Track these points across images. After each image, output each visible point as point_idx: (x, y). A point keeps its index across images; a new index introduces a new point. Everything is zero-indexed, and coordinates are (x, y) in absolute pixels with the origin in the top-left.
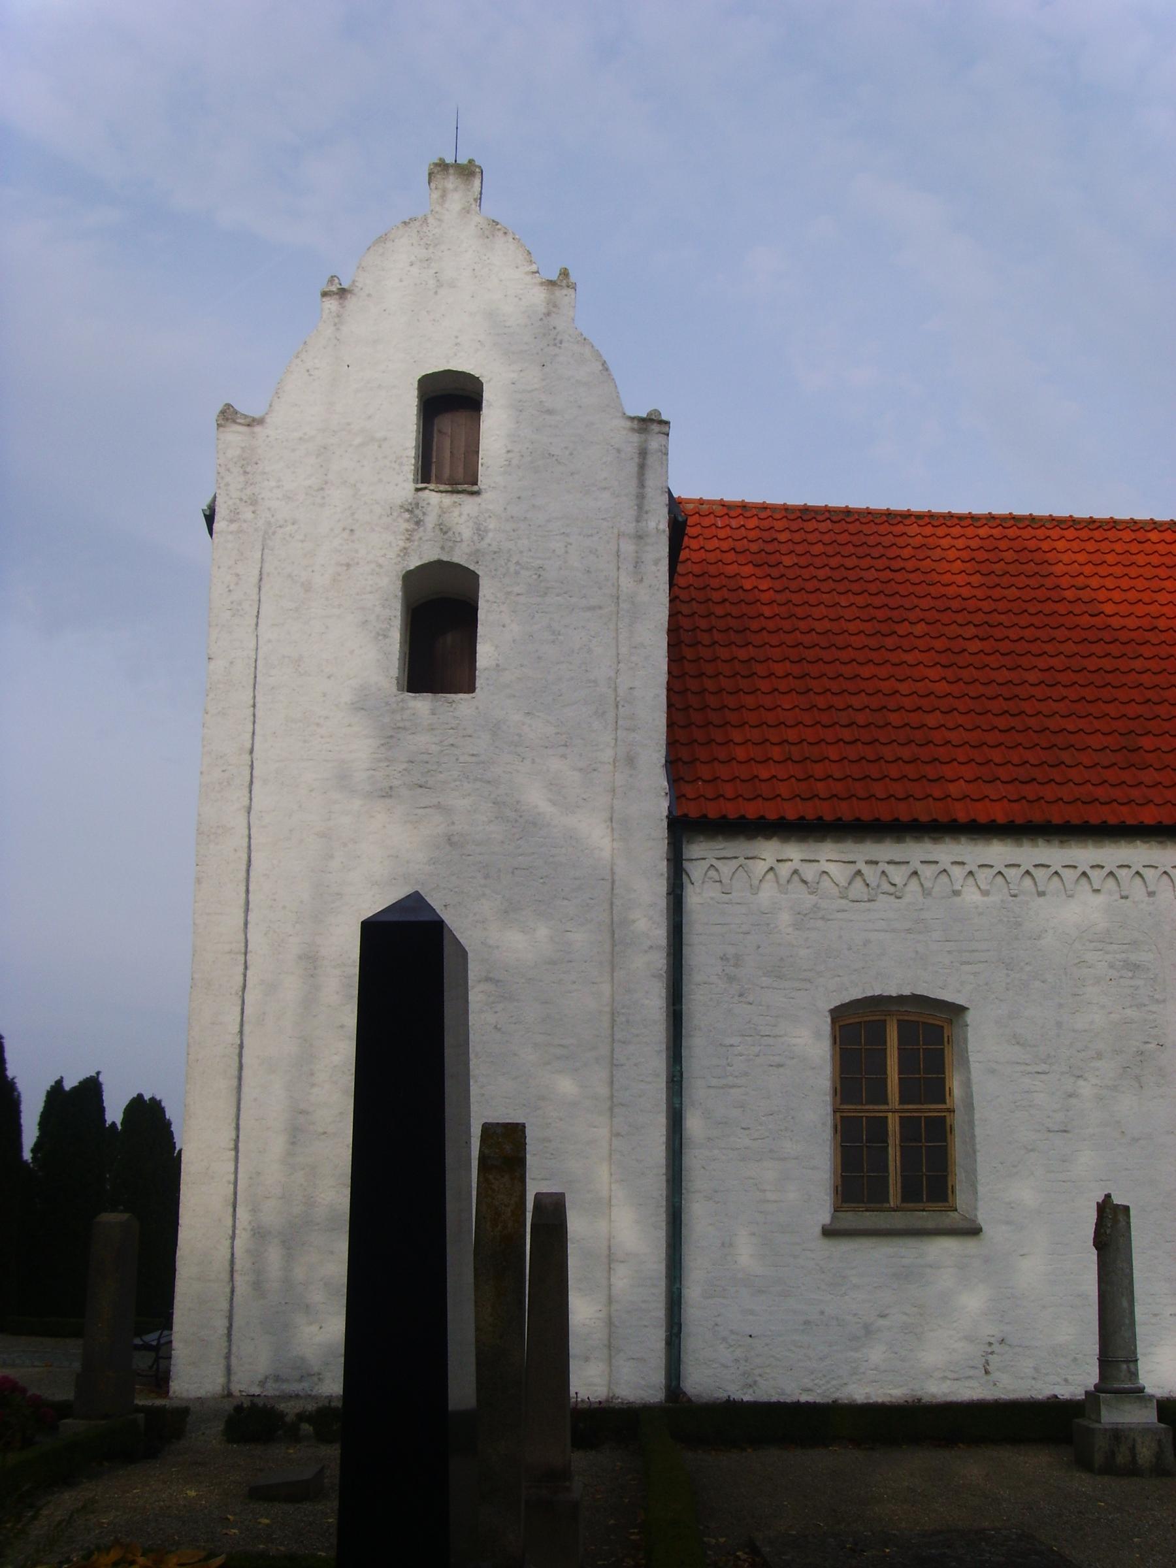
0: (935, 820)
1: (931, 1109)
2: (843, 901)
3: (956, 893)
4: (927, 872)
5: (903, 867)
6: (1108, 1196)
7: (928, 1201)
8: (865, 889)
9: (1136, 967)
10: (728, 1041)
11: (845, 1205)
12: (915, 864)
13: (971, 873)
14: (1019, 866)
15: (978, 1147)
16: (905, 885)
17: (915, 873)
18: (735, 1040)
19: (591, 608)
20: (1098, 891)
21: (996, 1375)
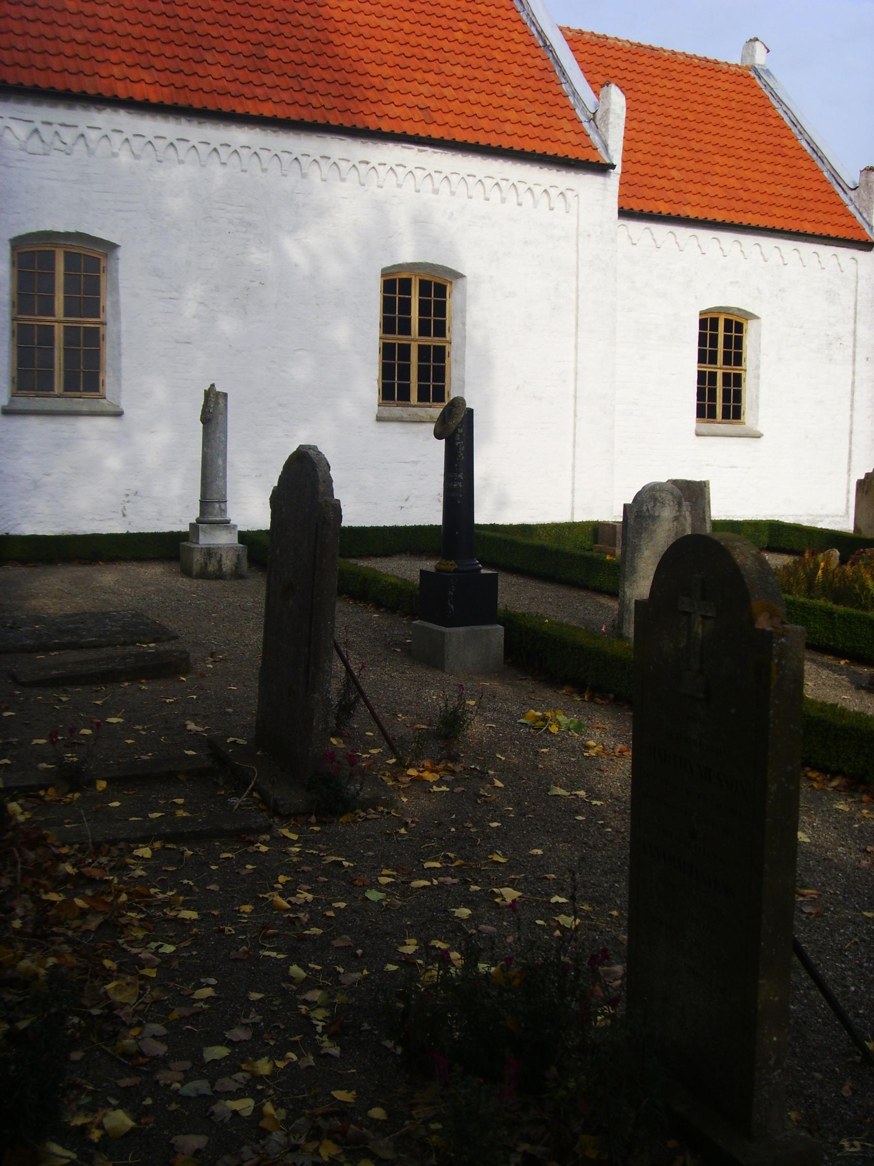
0: (100, 94)
1: (89, 322)
2: (22, 153)
3: (115, 155)
4: (93, 135)
5: (73, 130)
6: (213, 385)
7: (84, 391)
8: (40, 145)
11: (20, 392)
13: (127, 140)
14: (188, 141)
15: (123, 351)
16: (73, 145)
20: (224, 164)
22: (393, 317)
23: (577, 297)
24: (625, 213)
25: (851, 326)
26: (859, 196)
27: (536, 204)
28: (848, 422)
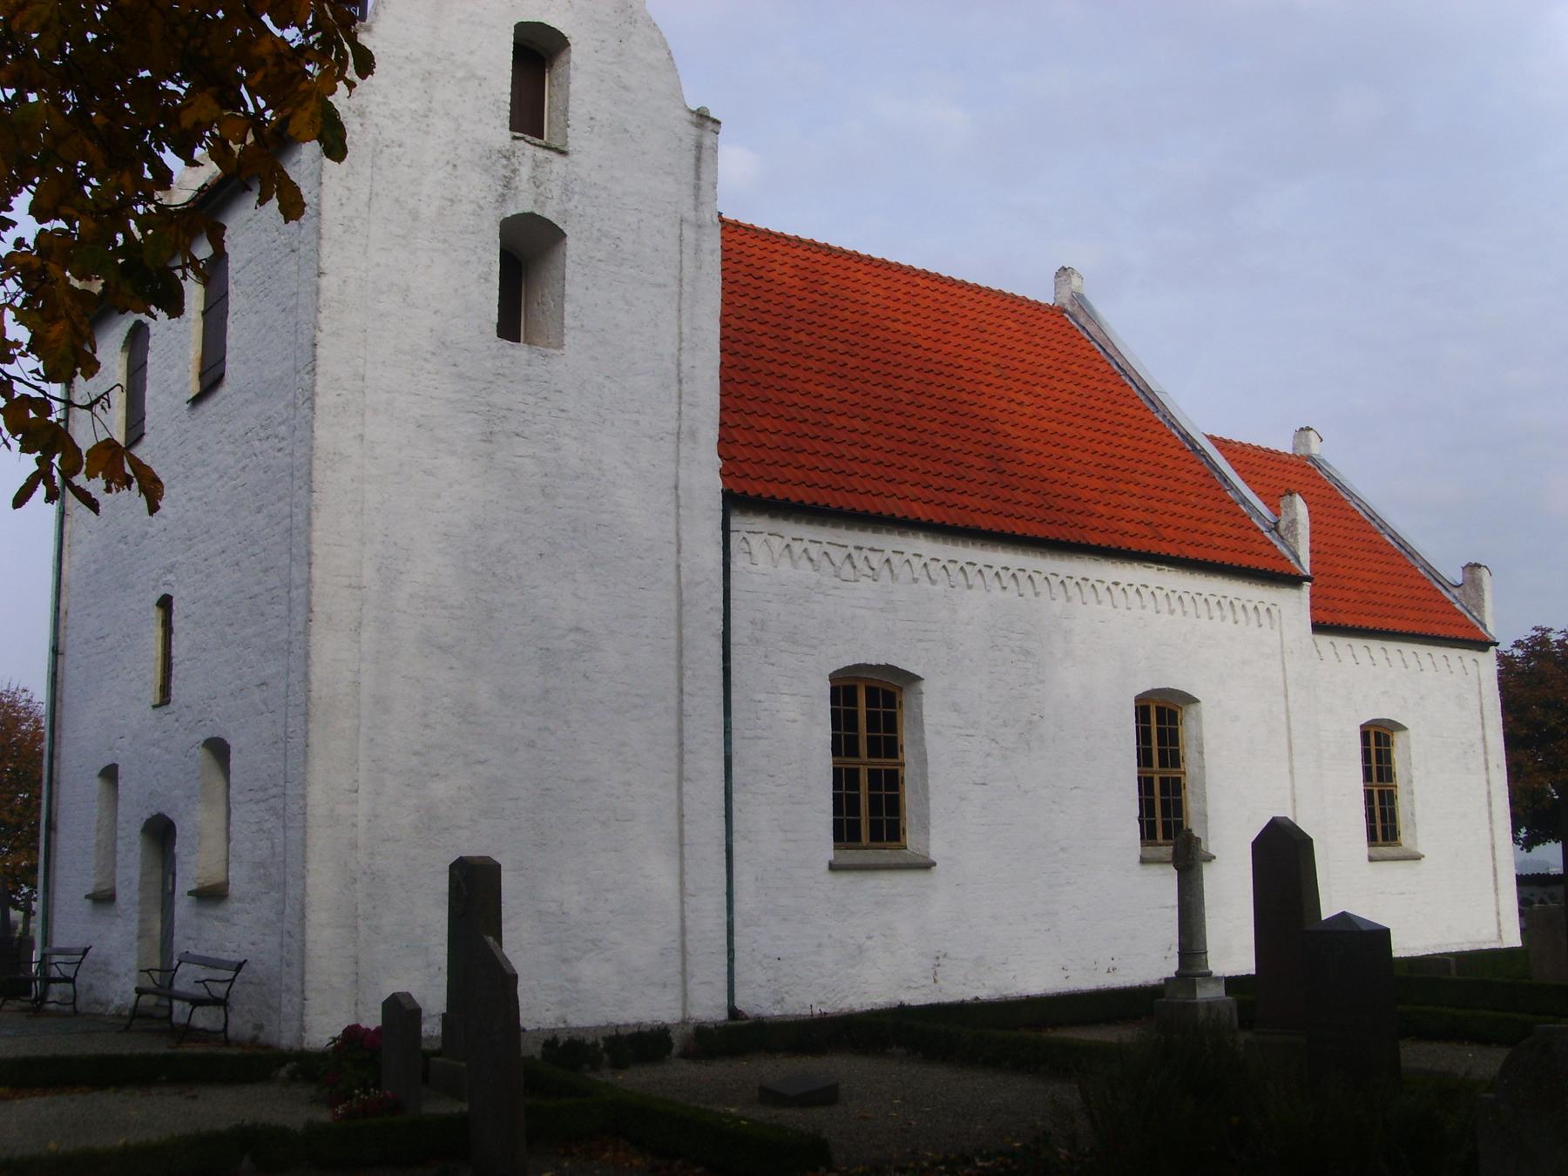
5: (879, 554)
9: (1027, 653)
10: (759, 697)
12: (851, 550)
17: (888, 561)
18: (762, 697)
19: (658, 285)
21: (941, 982)
22: (842, 719)
23: (1288, 718)
24: (1319, 627)
25: (1480, 732)
26: (1464, 593)
27: (1223, 618)
28: (1488, 836)
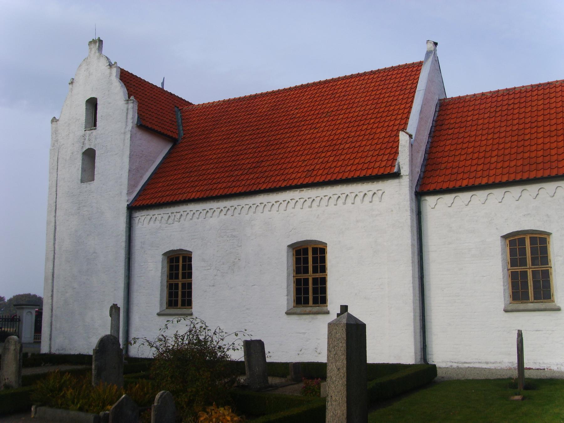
18: (143, 264)
19: (116, 154)
